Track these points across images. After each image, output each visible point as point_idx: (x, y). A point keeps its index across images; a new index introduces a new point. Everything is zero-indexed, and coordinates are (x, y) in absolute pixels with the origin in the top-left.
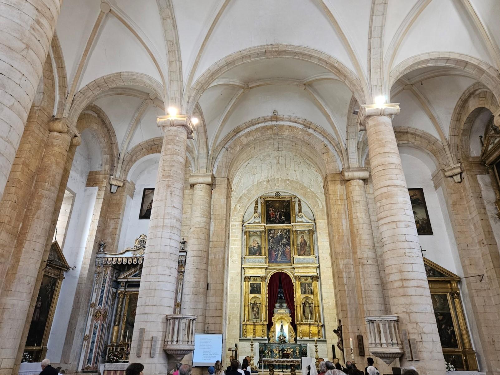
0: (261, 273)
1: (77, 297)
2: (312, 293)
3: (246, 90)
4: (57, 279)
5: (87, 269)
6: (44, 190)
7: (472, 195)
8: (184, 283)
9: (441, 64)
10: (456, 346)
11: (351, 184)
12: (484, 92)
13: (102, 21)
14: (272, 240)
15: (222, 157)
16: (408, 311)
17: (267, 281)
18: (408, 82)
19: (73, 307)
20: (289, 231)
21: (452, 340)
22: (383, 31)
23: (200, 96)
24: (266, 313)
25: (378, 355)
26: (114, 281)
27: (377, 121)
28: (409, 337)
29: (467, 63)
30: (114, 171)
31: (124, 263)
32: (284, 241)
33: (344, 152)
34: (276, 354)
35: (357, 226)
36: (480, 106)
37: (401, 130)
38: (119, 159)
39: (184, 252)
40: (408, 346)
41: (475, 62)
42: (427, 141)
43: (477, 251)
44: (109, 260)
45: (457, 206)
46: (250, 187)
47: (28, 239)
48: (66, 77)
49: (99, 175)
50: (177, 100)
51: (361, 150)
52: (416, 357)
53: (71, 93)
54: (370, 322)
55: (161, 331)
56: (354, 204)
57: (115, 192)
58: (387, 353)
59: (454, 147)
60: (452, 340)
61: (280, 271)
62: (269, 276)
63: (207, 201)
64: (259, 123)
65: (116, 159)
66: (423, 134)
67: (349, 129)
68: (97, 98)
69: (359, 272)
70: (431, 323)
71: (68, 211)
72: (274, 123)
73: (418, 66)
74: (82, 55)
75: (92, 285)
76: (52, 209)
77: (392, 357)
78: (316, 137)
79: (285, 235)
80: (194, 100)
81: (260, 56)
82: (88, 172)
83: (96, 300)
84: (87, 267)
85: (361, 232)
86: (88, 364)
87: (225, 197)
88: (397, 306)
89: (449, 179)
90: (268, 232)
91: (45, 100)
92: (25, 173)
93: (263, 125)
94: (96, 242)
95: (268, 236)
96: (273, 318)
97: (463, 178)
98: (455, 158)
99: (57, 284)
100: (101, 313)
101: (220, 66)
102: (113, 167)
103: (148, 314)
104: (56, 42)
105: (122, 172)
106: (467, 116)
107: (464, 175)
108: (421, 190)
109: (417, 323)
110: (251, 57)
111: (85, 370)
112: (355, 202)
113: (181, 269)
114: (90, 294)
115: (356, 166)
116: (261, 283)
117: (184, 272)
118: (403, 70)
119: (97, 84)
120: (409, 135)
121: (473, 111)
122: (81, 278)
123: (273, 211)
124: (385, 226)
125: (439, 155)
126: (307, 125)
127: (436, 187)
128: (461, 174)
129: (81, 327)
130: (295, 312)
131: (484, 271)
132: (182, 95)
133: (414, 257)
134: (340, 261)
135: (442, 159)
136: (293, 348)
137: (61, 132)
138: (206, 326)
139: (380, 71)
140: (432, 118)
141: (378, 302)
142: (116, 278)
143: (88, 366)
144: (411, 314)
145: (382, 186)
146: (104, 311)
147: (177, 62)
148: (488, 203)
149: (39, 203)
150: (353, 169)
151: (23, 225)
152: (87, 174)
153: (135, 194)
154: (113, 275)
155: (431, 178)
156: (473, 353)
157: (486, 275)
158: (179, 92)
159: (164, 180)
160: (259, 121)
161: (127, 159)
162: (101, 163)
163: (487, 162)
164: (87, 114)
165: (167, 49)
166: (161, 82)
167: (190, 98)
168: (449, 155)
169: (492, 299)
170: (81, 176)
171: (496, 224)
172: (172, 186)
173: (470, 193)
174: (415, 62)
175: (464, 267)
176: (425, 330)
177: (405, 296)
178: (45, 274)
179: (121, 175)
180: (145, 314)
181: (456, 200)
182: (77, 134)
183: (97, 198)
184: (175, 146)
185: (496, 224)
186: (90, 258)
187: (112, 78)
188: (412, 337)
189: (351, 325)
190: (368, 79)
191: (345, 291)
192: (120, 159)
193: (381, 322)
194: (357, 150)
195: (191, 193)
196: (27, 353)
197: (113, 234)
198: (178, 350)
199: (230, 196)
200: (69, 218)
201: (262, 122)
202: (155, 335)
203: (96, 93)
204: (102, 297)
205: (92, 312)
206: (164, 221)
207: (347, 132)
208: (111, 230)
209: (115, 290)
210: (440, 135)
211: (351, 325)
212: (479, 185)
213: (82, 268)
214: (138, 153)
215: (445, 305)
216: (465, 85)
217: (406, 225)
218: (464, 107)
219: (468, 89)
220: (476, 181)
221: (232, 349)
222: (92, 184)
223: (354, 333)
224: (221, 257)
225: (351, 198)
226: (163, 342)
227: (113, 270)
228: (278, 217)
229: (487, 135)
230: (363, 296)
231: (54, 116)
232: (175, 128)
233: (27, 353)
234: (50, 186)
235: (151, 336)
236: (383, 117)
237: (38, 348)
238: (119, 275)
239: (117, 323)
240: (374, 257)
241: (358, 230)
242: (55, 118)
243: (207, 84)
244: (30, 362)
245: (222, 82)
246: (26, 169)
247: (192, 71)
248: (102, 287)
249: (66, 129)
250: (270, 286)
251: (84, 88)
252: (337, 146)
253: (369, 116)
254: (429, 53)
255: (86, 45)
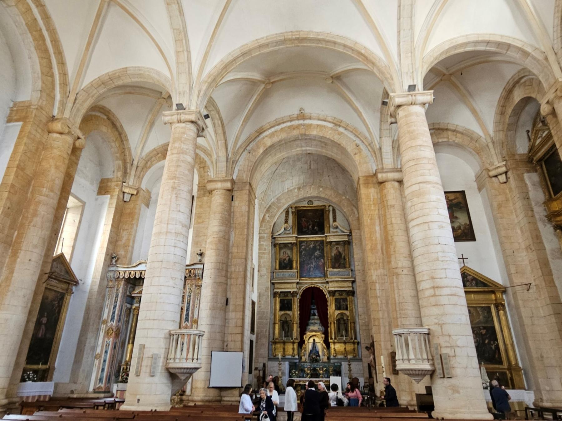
0: (292, 288)
1: (87, 313)
2: (347, 309)
3: (267, 85)
4: (64, 293)
5: (98, 283)
6: (41, 195)
7: (518, 195)
8: (201, 298)
9: (481, 48)
10: (501, 363)
11: (385, 187)
12: (530, 79)
13: (104, 11)
14: (304, 252)
15: (244, 160)
16: (440, 322)
17: (298, 296)
18: (445, 71)
19: (83, 323)
20: (322, 242)
21: (497, 356)
22: (413, 10)
23: (213, 90)
24: (297, 331)
25: (405, 372)
26: (128, 296)
27: (408, 111)
28: (441, 351)
29: (509, 46)
30: (127, 178)
31: (137, 277)
32: (317, 253)
33: (378, 153)
34: (308, 374)
35: (392, 232)
36: (526, 96)
37: (441, 127)
38: (132, 165)
39: (201, 264)
40: (440, 361)
41: (519, 45)
42: (469, 139)
43: (524, 258)
44: (121, 274)
45: (503, 209)
46: (279, 195)
47: (23, 248)
48: (68, 74)
49: (111, 182)
50: (185, 95)
51: (396, 149)
52: (448, 374)
53: (72, 90)
54: (398, 336)
55: (163, 348)
56: (388, 209)
57: (128, 200)
58: (415, 370)
59: (498, 144)
60: (497, 356)
61: (313, 286)
62: (301, 291)
63: (226, 208)
64: (284, 123)
65: (129, 165)
66: (465, 130)
67: (382, 125)
68: (102, 97)
69: (393, 283)
70: (466, 336)
71: (77, 222)
72: (301, 122)
73: (455, 51)
74: (84, 49)
75: (103, 300)
76: (51, 217)
77: (421, 375)
78: (347, 136)
79: (318, 247)
80: (205, 94)
81: (279, 45)
82: (100, 180)
83: (108, 316)
84: (98, 280)
85: (396, 239)
86: (99, 384)
87: (247, 203)
88: (428, 317)
89: (494, 179)
90: (300, 244)
91: (44, 99)
92: (20, 178)
93: (289, 124)
94: (107, 254)
95: (300, 249)
96: (304, 337)
97: (509, 178)
98: (500, 156)
99: (65, 300)
100: (113, 330)
101: (235, 56)
102: (125, 173)
103: (148, 329)
104: (55, 36)
105: (135, 180)
106: (512, 108)
107: (509, 174)
108: (463, 193)
109: (450, 336)
110: (269, 46)
111: (97, 390)
112: (389, 207)
113: (198, 283)
114: (101, 309)
115: (390, 167)
116: (291, 299)
117: (201, 286)
118: (437, 56)
119: (102, 82)
120: (450, 133)
121: (519, 102)
122: (91, 292)
123: (305, 221)
124: (416, 228)
125: (482, 153)
126: (337, 124)
127: (480, 189)
128: (506, 173)
129: (92, 345)
130: (329, 329)
131: (532, 279)
132: (191, 88)
133: (448, 262)
134: (372, 271)
135: (486, 158)
136: (326, 367)
137: (61, 133)
138: (225, 344)
139: (411, 56)
140: (474, 112)
141: (414, 315)
142: (130, 293)
143: (100, 386)
144: (444, 326)
145: (413, 184)
146: (117, 328)
147: (185, 53)
148: (536, 205)
149: (36, 210)
150: (387, 170)
151: (18, 233)
152: (98, 182)
153: (151, 202)
154: (126, 290)
155: (475, 179)
156: (519, 369)
157: (533, 284)
158: (188, 86)
159: (169, 181)
160: (285, 120)
161: (141, 165)
162: (113, 169)
163: (535, 158)
164: (95, 116)
165: (174, 38)
166: (169, 75)
167: (200, 92)
168: (493, 152)
169: (541, 310)
170: (92, 183)
171: (545, 227)
172: (178, 188)
173: (516, 194)
174: (452, 45)
175: (509, 275)
176: (459, 343)
177: (437, 305)
178: (47, 286)
179: (135, 182)
180: (145, 329)
181: (501, 202)
182: (81, 136)
183: (109, 207)
184: (182, 144)
185: (545, 227)
186: (101, 271)
187: (117, 74)
188: (444, 351)
189: (384, 341)
190: (399, 66)
191: (378, 304)
192: (133, 165)
193: (410, 335)
194: (391, 150)
195: (209, 201)
196: (31, 372)
197: (126, 246)
198: (181, 368)
199: (254, 204)
200: (78, 228)
201: (287, 121)
202: (156, 352)
203: (101, 92)
204: (114, 313)
205: (104, 329)
206: (167, 227)
207: (380, 129)
208: (124, 241)
209: (129, 306)
210: (483, 130)
211: (384, 341)
212: (526, 185)
213: (93, 282)
214: (153, 159)
215: (489, 317)
216: (509, 73)
217: (439, 226)
218: (509, 99)
219: (512, 77)
220: (522, 180)
221: (258, 369)
222: (103, 192)
223: (388, 349)
224: (241, 269)
225: (385, 202)
226: (166, 359)
227: (125, 285)
228: (310, 227)
229: (535, 129)
230: (398, 309)
231: (54, 116)
232: (183, 125)
233: (31, 372)
234: (49, 192)
235: (151, 353)
236: (414, 106)
237: (44, 367)
238: (134, 290)
239: (131, 340)
240: (410, 265)
241: (393, 237)
242: (55, 118)
243: (220, 77)
244: (35, 381)
245: (239, 76)
246: (21, 173)
247: (202, 62)
248: (115, 302)
249: (66, 130)
250: (301, 301)
251: (87, 85)
252: (370, 145)
253: (399, 106)
254: (466, 36)
255: (87, 39)
